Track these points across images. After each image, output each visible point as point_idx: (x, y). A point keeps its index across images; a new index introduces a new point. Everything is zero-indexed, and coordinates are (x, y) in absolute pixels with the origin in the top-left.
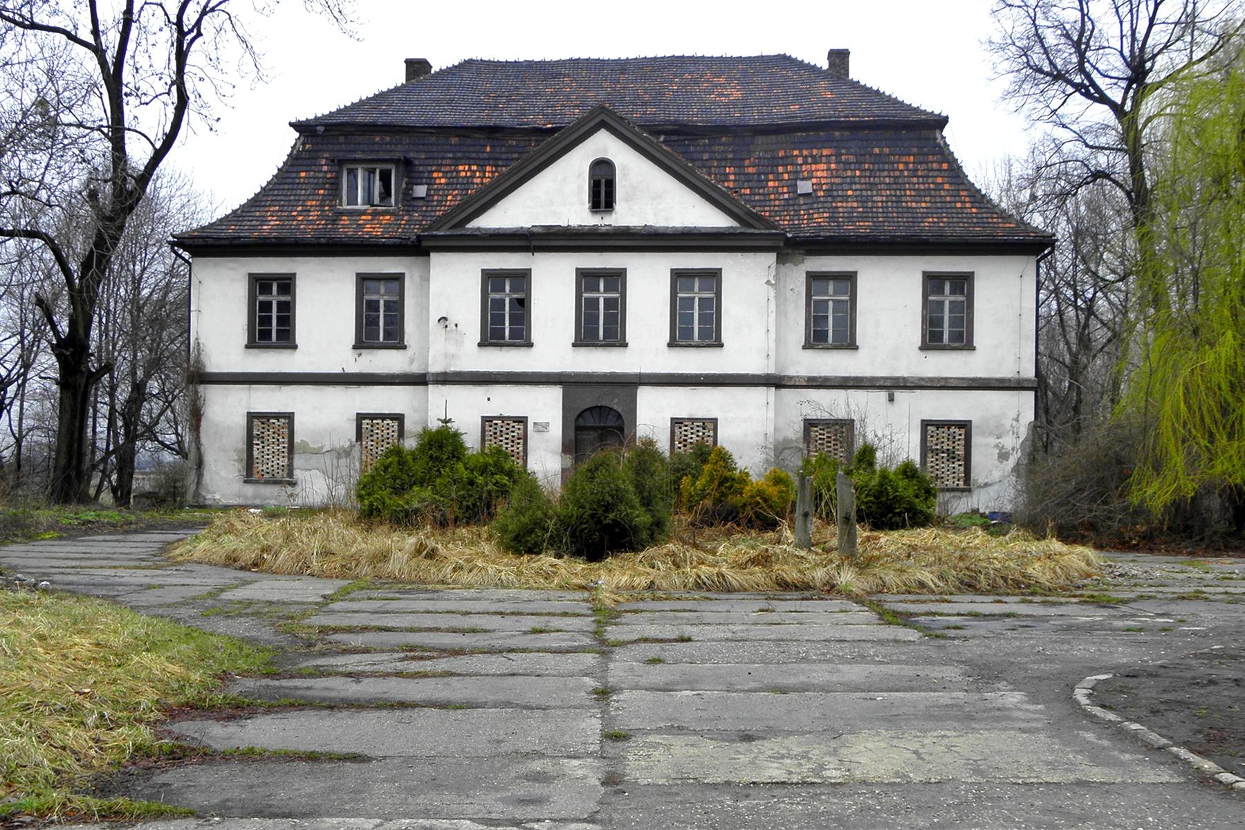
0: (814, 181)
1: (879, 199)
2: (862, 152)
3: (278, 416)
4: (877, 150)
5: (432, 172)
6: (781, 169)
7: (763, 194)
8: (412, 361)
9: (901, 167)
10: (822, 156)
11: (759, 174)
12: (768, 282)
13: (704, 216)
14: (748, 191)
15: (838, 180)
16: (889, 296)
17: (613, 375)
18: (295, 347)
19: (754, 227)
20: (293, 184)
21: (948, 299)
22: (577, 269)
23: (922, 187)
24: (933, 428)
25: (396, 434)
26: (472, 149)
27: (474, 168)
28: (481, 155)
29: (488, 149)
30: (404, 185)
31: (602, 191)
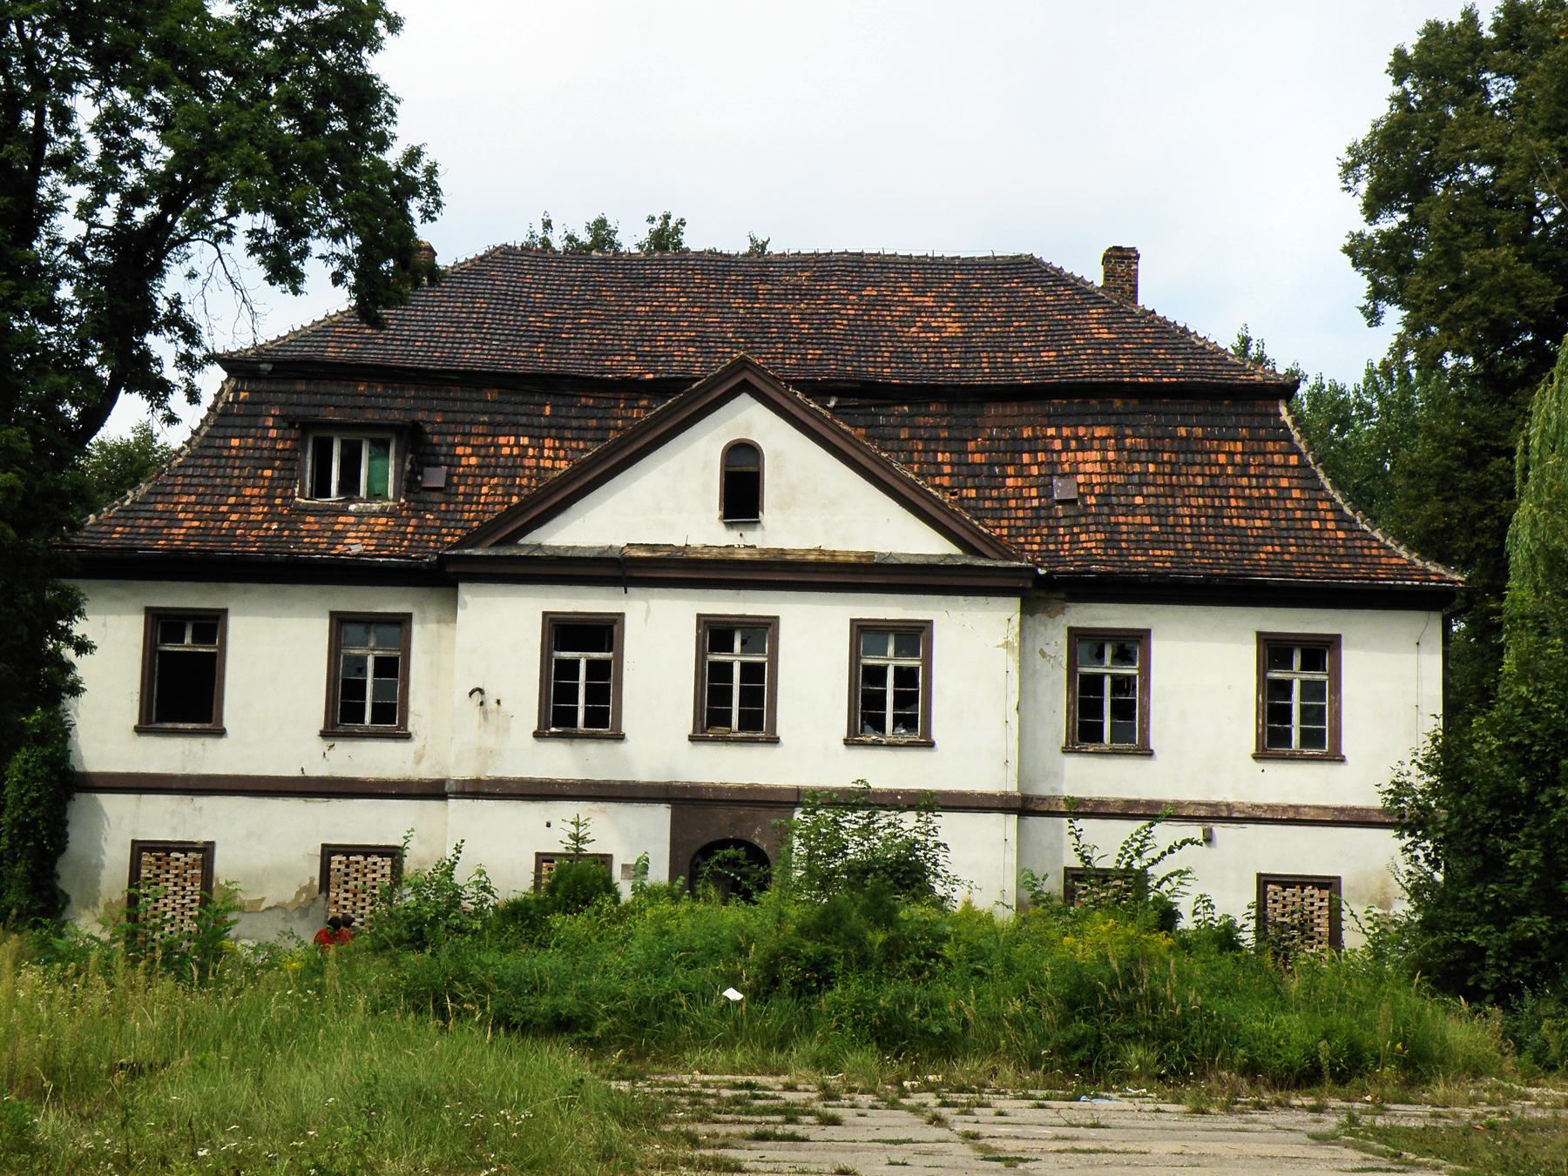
0: (1081, 479)
1: (1186, 511)
2: (1159, 432)
3: (185, 847)
4: (1182, 431)
5: (455, 445)
6: (1026, 458)
7: (998, 499)
8: (419, 759)
9: (1222, 459)
10: (1093, 438)
11: (991, 465)
12: (1007, 645)
13: (912, 539)
14: (973, 493)
15: (1118, 479)
16: (1203, 672)
17: (754, 789)
18: (220, 733)
19: (985, 556)
20: (220, 457)
21: (1297, 677)
22: (699, 616)
23: (1256, 493)
24: (1278, 888)
25: (387, 882)
26: (522, 409)
27: (525, 441)
28: (535, 421)
29: (548, 410)
30: (408, 467)
31: (742, 492)
